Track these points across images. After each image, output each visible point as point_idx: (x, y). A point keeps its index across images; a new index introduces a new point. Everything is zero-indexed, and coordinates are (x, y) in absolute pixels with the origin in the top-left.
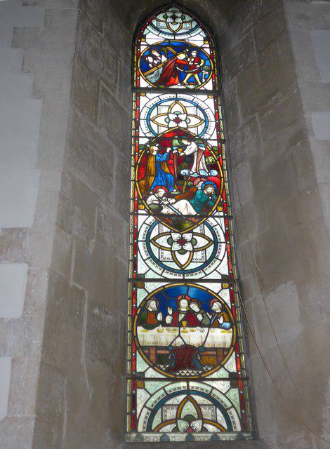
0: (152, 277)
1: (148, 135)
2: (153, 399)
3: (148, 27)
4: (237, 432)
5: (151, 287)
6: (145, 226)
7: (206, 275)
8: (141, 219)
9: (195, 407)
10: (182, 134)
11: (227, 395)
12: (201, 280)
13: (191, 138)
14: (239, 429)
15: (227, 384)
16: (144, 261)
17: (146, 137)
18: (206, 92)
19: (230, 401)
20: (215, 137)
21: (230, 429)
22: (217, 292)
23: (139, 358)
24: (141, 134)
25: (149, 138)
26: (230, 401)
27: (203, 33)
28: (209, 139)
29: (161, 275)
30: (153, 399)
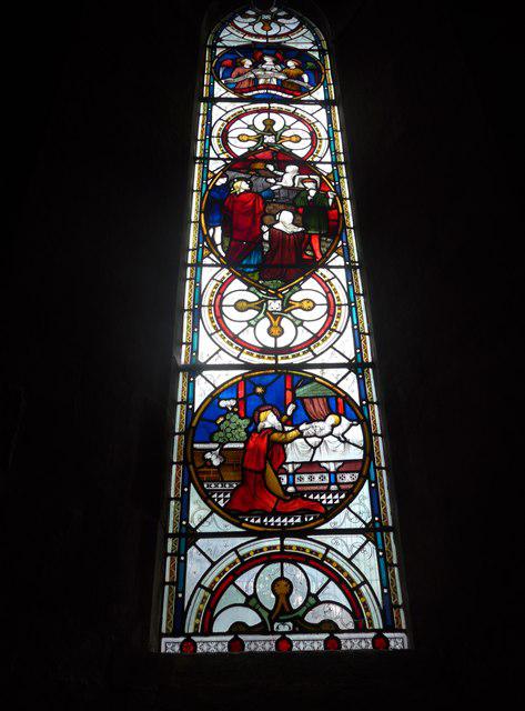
0: (227, 363)
1: (223, 156)
2: (227, 347)
3: (229, 28)
4: (374, 630)
5: (221, 378)
6: (221, 122)
7: (316, 356)
8: (207, 273)
9: (345, 593)
10: (283, 158)
11: (353, 561)
12: (304, 365)
13: (290, 158)
14: (378, 623)
15: (360, 539)
16: (210, 336)
17: (219, 159)
18: (316, 102)
19: (226, 554)
20: (328, 158)
21: (360, 627)
22: (209, 565)
23: (194, 496)
24: (212, 155)
25: (224, 160)
26: (226, 554)
27: (309, 34)
28: (320, 162)
29: (237, 358)
30: (227, 347)
